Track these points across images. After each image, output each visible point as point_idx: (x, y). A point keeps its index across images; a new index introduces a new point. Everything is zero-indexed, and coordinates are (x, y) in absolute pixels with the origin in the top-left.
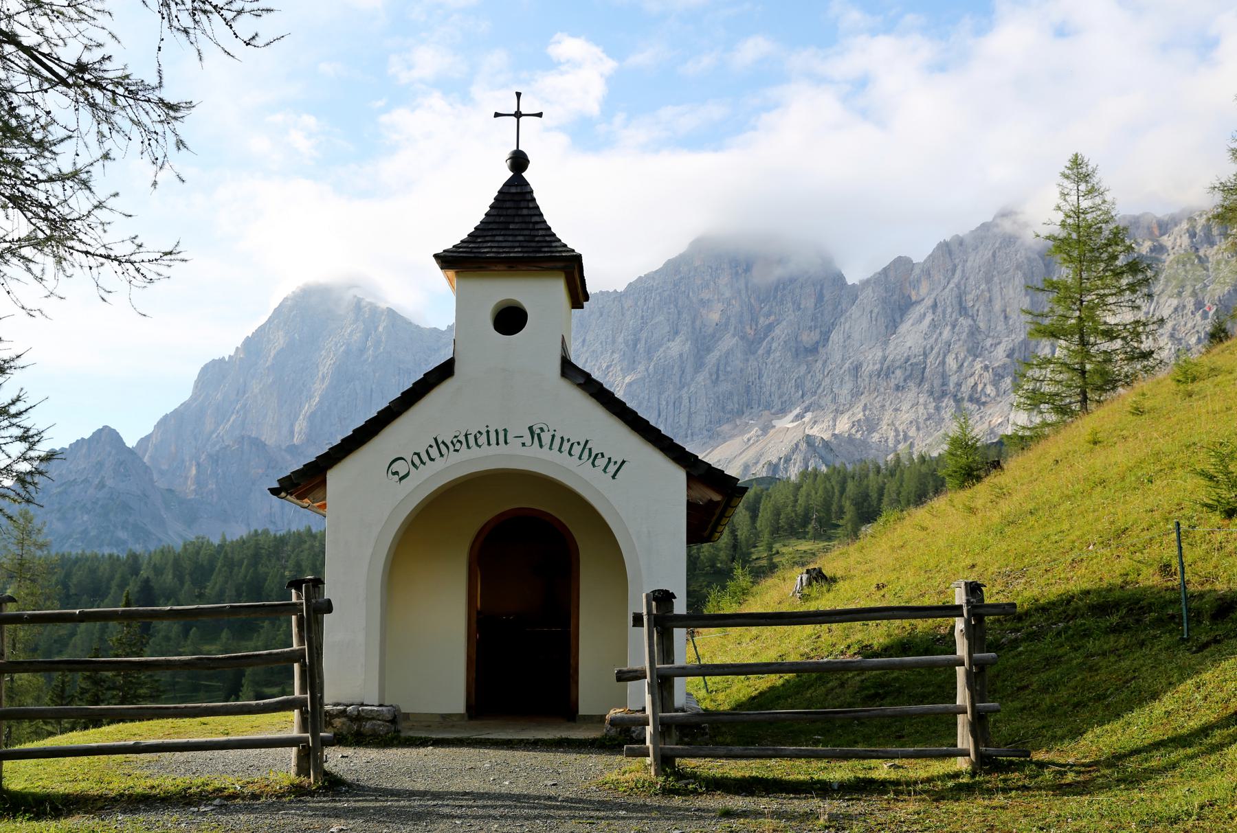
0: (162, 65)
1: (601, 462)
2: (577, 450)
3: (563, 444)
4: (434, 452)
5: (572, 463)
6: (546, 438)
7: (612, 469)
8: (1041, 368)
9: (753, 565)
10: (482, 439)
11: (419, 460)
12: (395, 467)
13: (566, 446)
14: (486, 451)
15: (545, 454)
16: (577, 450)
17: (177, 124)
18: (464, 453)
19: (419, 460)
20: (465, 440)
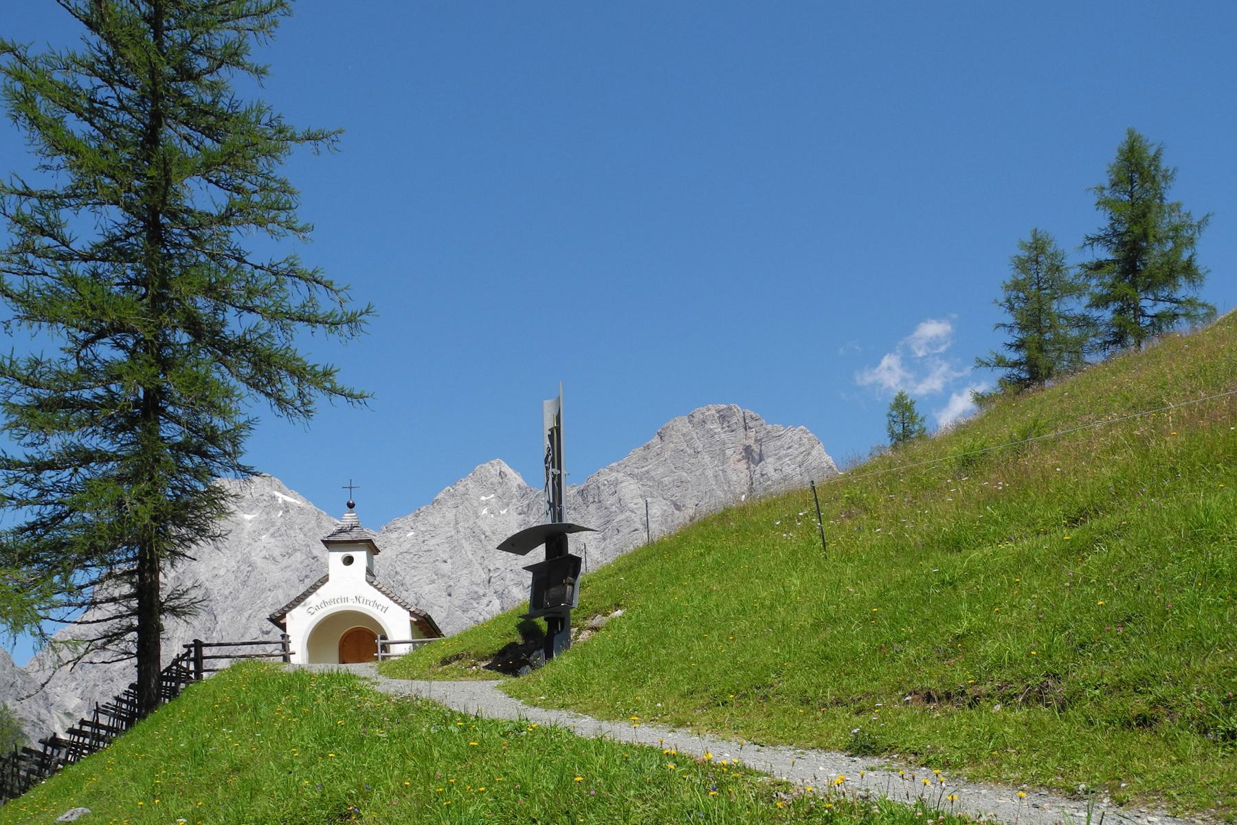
0: (4, 304)
2: (372, 604)
3: (367, 602)
4: (323, 605)
5: (370, 608)
6: (361, 600)
7: (384, 610)
8: (197, 534)
9: (1109, 560)
10: (339, 601)
11: (317, 608)
12: (310, 610)
14: (337, 605)
15: (361, 605)
16: (372, 604)
17: (39, 358)
19: (317, 608)
20: (334, 601)
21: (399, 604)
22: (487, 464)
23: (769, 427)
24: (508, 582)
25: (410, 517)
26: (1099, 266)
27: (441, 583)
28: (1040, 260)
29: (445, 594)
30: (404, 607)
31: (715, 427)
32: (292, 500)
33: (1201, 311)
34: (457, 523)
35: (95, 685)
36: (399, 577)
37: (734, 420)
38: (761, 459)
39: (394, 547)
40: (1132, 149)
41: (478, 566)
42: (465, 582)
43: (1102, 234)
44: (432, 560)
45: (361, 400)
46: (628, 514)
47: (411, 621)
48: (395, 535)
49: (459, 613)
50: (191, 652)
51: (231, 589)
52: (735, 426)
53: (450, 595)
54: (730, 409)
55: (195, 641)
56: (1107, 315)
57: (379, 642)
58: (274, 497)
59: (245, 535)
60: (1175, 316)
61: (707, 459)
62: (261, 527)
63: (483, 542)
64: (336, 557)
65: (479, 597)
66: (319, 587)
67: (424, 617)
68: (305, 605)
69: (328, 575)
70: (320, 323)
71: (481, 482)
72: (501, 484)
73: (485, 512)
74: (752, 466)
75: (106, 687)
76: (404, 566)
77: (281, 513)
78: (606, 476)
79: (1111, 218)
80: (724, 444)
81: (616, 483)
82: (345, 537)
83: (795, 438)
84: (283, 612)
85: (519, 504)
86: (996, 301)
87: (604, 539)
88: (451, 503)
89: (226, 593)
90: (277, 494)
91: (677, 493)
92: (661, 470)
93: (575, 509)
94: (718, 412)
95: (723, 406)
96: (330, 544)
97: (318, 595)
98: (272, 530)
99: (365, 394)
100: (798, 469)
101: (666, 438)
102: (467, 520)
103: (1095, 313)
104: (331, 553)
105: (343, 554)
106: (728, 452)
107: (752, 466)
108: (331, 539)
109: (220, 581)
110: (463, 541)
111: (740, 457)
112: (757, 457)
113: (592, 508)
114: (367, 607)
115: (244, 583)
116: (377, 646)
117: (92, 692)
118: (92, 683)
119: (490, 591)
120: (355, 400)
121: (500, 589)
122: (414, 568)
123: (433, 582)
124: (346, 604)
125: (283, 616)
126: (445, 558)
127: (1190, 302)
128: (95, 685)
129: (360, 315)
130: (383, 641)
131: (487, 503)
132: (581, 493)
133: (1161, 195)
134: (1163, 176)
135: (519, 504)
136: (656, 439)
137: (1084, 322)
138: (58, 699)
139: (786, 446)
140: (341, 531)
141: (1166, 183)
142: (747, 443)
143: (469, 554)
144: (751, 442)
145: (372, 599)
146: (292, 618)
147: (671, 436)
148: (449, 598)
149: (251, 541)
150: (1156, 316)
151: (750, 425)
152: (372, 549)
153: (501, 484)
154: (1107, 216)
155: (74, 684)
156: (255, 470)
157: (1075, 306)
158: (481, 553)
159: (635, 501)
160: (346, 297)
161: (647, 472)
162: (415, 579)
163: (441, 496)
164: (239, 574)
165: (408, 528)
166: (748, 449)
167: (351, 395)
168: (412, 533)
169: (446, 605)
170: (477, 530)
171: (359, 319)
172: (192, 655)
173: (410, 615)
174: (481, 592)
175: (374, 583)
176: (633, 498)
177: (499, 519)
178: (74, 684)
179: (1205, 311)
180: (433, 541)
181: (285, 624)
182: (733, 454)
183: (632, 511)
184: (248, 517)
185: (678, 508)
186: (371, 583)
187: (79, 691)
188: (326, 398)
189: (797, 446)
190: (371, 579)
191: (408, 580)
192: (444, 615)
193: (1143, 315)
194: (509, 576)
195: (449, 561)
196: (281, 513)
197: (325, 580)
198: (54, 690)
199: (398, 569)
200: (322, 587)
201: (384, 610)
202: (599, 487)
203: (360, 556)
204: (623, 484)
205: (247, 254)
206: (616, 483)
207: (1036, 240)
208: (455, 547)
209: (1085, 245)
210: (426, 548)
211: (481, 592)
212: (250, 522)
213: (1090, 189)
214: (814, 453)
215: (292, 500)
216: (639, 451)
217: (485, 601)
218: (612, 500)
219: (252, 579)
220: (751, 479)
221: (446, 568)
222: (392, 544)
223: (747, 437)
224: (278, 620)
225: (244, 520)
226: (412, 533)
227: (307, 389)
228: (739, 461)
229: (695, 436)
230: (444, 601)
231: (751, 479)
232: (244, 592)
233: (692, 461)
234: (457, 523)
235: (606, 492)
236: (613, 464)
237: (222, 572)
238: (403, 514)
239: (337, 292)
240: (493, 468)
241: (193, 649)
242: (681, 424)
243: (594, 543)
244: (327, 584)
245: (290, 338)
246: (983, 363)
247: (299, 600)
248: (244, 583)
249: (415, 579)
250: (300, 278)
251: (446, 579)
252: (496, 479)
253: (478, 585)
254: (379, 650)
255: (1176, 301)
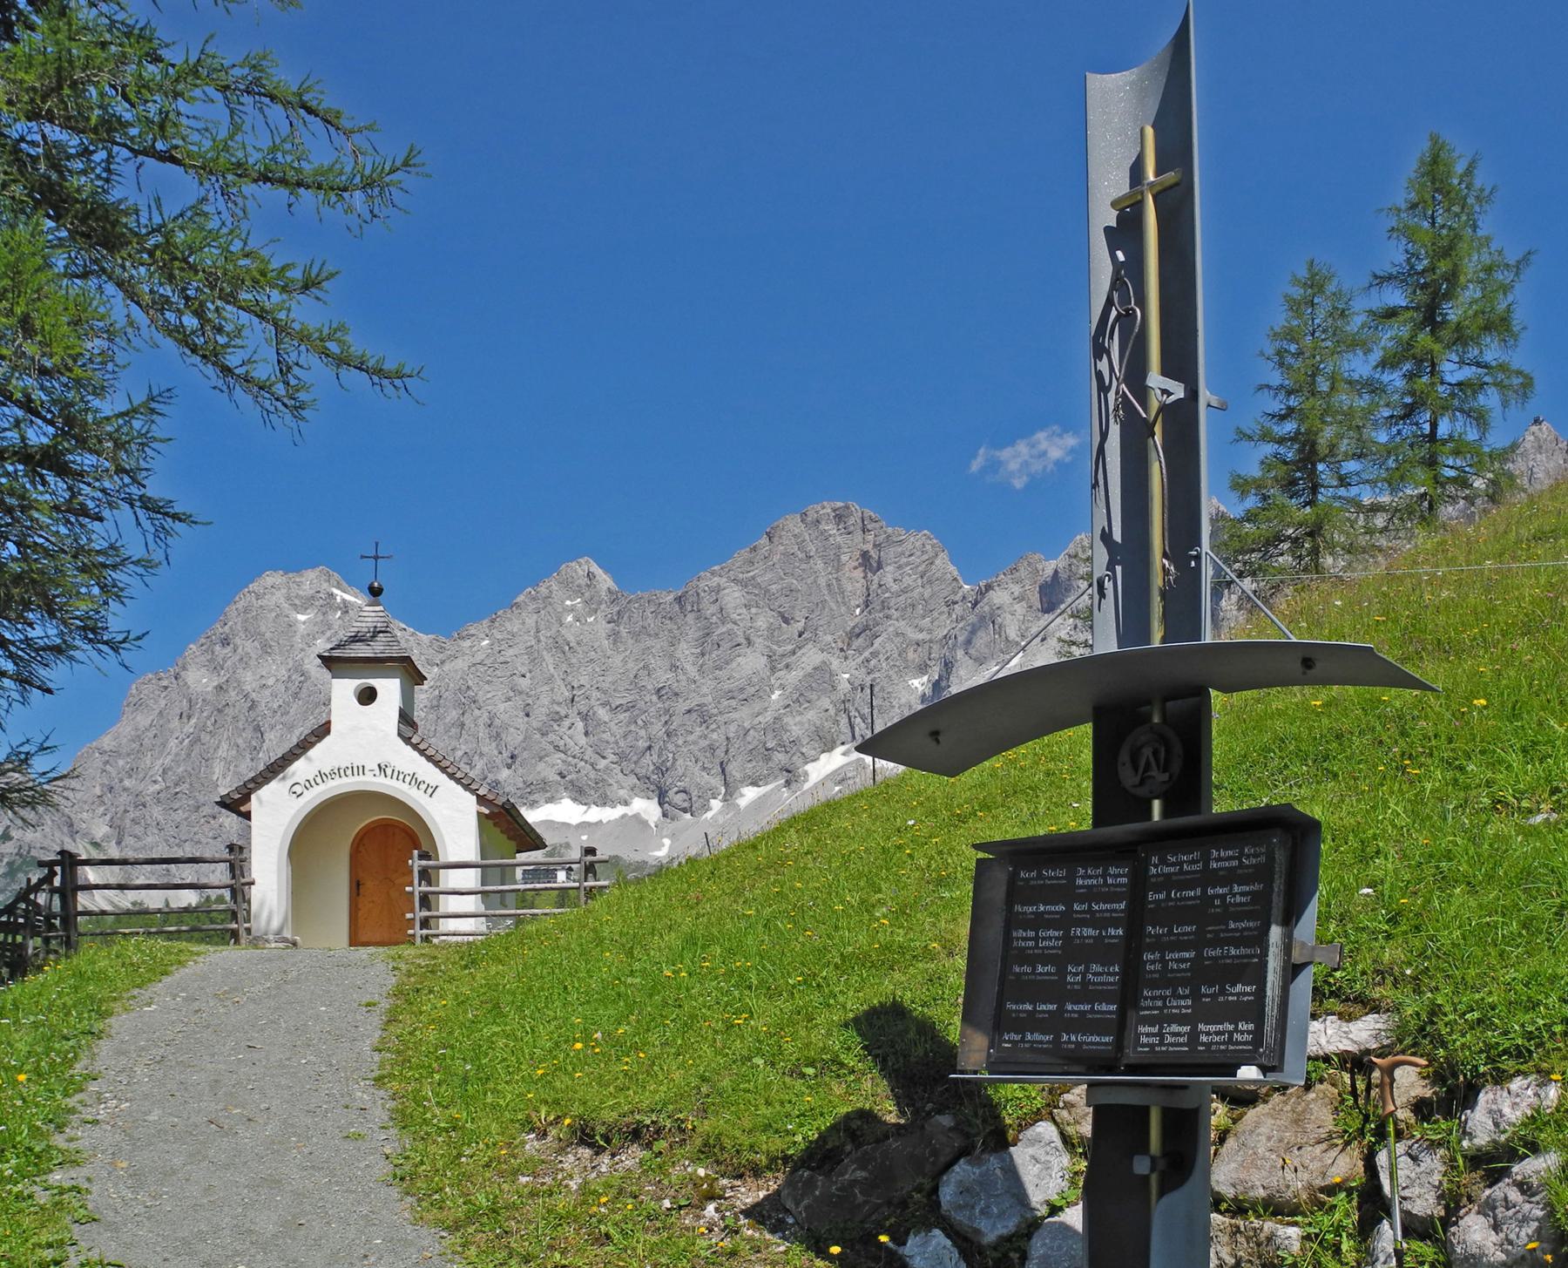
1: (423, 787)
2: (408, 779)
3: (399, 775)
4: (319, 780)
5: (405, 787)
6: (389, 771)
7: (430, 791)
10: (349, 772)
11: (309, 784)
12: (294, 789)
13: (401, 777)
15: (388, 781)
16: (408, 779)
18: (337, 782)
19: (309, 784)
20: (338, 772)
21: (458, 781)
22: (574, 564)
23: (890, 530)
24: (593, 702)
25: (486, 622)
26: (1391, 313)
27: (519, 701)
28: (1316, 301)
29: (522, 714)
30: (466, 787)
31: (831, 528)
32: (352, 599)
33: (1516, 381)
34: (538, 631)
35: (126, 811)
36: (471, 693)
37: (851, 521)
38: (880, 567)
39: (466, 658)
40: (1435, 160)
41: (559, 682)
42: (545, 700)
43: (1394, 271)
44: (508, 674)
45: (398, 382)
46: (730, 626)
47: (479, 813)
48: (467, 643)
49: (538, 736)
50: (55, 874)
51: (281, 703)
52: (852, 528)
53: (528, 715)
54: (848, 508)
55: (62, 853)
56: (1395, 379)
57: (416, 864)
58: (332, 595)
59: (298, 639)
60: (1482, 385)
61: (820, 565)
62: (316, 629)
63: (568, 654)
64: (344, 690)
65: (561, 719)
66: (312, 745)
67: (503, 806)
68: (284, 778)
69: (329, 722)
70: (308, 187)
71: (567, 584)
72: (588, 586)
73: (570, 619)
74: (869, 575)
75: (138, 814)
76: (477, 680)
77: (339, 614)
78: (708, 581)
79: (1407, 251)
80: (839, 547)
81: (718, 589)
82: (361, 651)
83: (918, 544)
84: (246, 791)
85: (609, 611)
86: (1262, 354)
87: (703, 655)
88: (532, 607)
89: (275, 706)
90: (336, 591)
91: (785, 603)
92: (769, 576)
93: (671, 618)
94: (834, 511)
95: (840, 504)
96: (333, 663)
97: (309, 759)
98: (328, 634)
99: (407, 370)
100: (919, 581)
101: (775, 539)
102: (548, 628)
103: (1386, 378)
104: (335, 681)
105: (357, 682)
106: (844, 558)
107: (869, 575)
108: (336, 653)
109: (267, 692)
110: (545, 653)
111: (856, 564)
112: (875, 565)
113: (690, 618)
114: (399, 785)
115: (296, 695)
116: (412, 871)
117: (122, 819)
118: (122, 808)
119: (573, 713)
120: (386, 382)
121: (584, 710)
122: (488, 682)
123: (509, 699)
124: (361, 778)
125: (246, 798)
126: (523, 672)
127: (1503, 367)
128: (126, 811)
129: (392, 171)
130: (424, 863)
131: (572, 609)
132: (679, 600)
133: (1474, 221)
134: (1477, 198)
135: (609, 611)
136: (764, 540)
137: (1373, 387)
138: (84, 826)
139: (907, 553)
140: (356, 639)
141: (1481, 206)
142: (865, 548)
143: (551, 667)
144: (869, 547)
145: (408, 769)
146: (260, 801)
147: (780, 537)
148: (526, 719)
149: (305, 646)
150: (1459, 384)
151: (869, 527)
152: (411, 674)
153: (588, 586)
154: (1401, 248)
155: (102, 809)
156: (178, 508)
157: (1360, 366)
158: (564, 667)
159: (739, 611)
160: (366, 146)
161: (753, 578)
162: (489, 695)
163: (520, 598)
164: (290, 685)
165: (483, 636)
166: (865, 555)
167: (379, 372)
168: (487, 642)
169: (523, 727)
170: (560, 640)
171: (387, 179)
172: (57, 881)
173: (478, 803)
174: (563, 713)
175: (413, 741)
176: (736, 608)
177: (586, 628)
178: (102, 809)
179: (1520, 380)
180: (511, 652)
181: (250, 812)
182: (849, 559)
183: (735, 623)
184: (301, 618)
185: (786, 621)
186: (407, 740)
187: (108, 818)
188: (330, 372)
189: (919, 553)
190: (408, 732)
191: (481, 697)
192: (521, 738)
193: (1442, 383)
194: (595, 694)
195: (528, 675)
196: (339, 614)
197: (324, 730)
198: (80, 816)
199: (470, 683)
200: (318, 746)
201: (430, 791)
202: (698, 594)
203: (389, 689)
204: (726, 591)
205: (167, 46)
206: (718, 589)
207: (1313, 276)
208: (535, 659)
209: (1371, 286)
210: (502, 659)
211: (563, 713)
212: (304, 623)
213: (1382, 210)
214: (938, 562)
215: (352, 599)
216: (745, 553)
217: (567, 723)
218: (713, 609)
219: (304, 690)
220: (868, 589)
221: (524, 683)
222: (464, 654)
223: (865, 542)
224: (237, 804)
225: (297, 621)
226: (487, 642)
227: (294, 356)
228: (855, 568)
229: (807, 537)
230: (521, 721)
231: (868, 589)
232: (295, 706)
233: (804, 566)
234: (538, 631)
235: (706, 599)
236: (716, 568)
237: (271, 682)
238: (478, 619)
239: (348, 134)
240: (581, 568)
241: (58, 869)
242: (793, 524)
243: (691, 659)
244: (327, 740)
245: (241, 214)
246: (1245, 435)
247: (275, 769)
248: (296, 695)
249: (489, 695)
250: (273, 98)
251: (524, 696)
252: (584, 581)
253: (559, 704)
254: (416, 881)
255: (1486, 366)
